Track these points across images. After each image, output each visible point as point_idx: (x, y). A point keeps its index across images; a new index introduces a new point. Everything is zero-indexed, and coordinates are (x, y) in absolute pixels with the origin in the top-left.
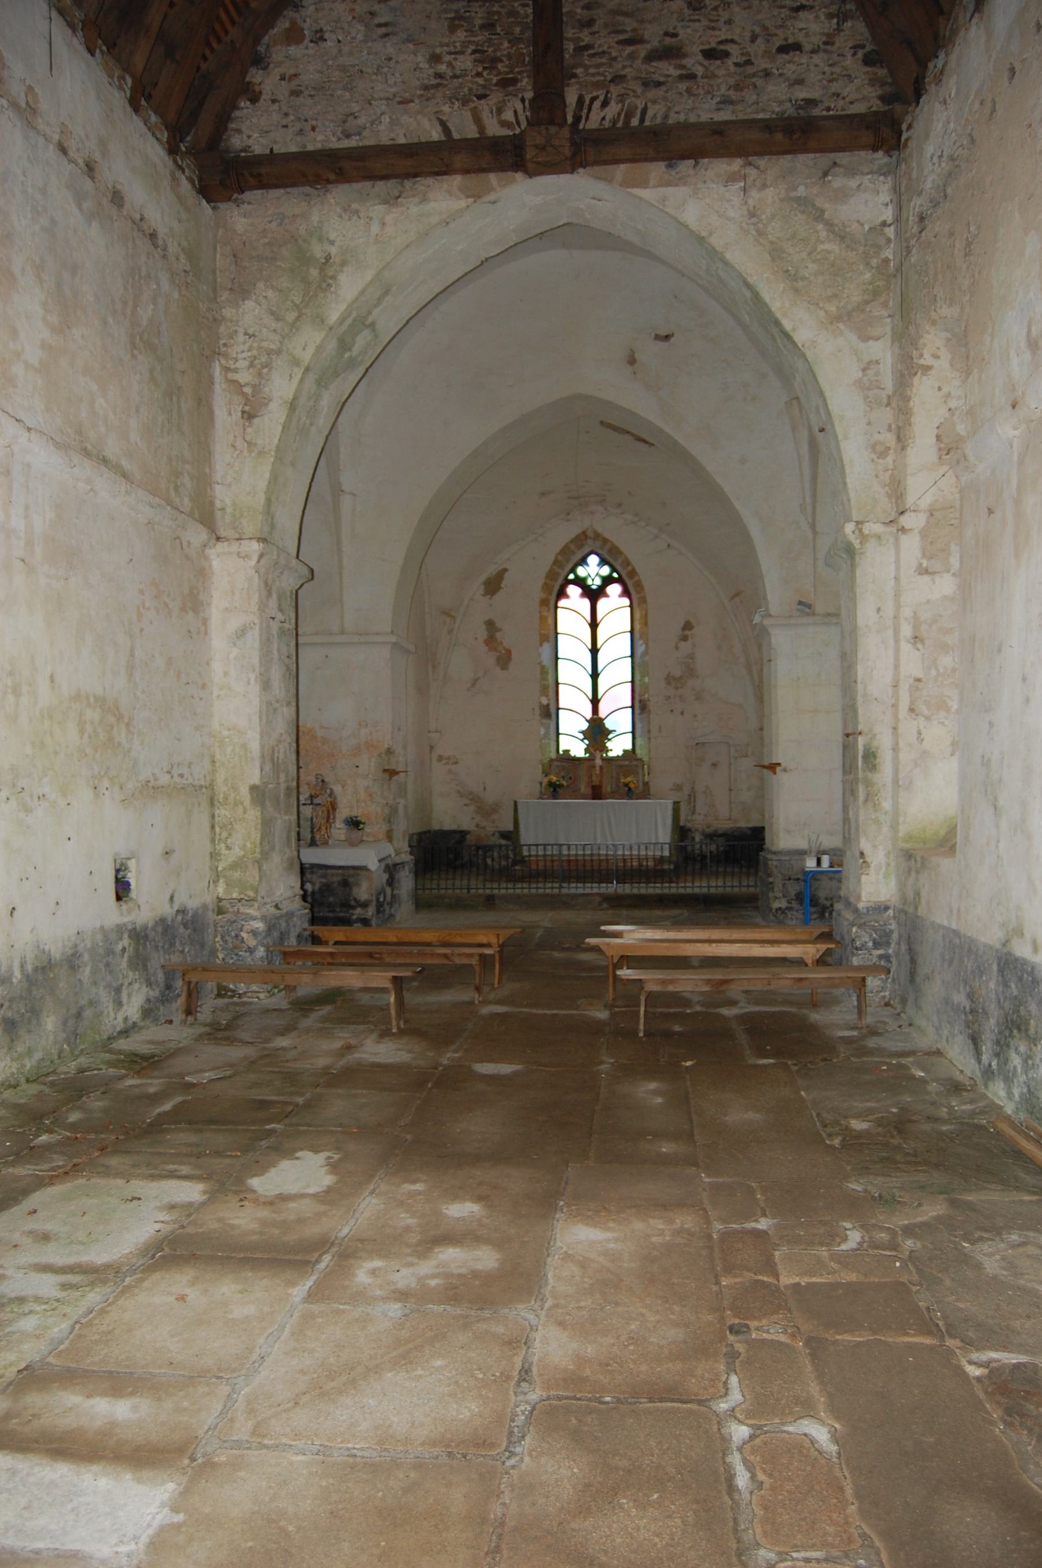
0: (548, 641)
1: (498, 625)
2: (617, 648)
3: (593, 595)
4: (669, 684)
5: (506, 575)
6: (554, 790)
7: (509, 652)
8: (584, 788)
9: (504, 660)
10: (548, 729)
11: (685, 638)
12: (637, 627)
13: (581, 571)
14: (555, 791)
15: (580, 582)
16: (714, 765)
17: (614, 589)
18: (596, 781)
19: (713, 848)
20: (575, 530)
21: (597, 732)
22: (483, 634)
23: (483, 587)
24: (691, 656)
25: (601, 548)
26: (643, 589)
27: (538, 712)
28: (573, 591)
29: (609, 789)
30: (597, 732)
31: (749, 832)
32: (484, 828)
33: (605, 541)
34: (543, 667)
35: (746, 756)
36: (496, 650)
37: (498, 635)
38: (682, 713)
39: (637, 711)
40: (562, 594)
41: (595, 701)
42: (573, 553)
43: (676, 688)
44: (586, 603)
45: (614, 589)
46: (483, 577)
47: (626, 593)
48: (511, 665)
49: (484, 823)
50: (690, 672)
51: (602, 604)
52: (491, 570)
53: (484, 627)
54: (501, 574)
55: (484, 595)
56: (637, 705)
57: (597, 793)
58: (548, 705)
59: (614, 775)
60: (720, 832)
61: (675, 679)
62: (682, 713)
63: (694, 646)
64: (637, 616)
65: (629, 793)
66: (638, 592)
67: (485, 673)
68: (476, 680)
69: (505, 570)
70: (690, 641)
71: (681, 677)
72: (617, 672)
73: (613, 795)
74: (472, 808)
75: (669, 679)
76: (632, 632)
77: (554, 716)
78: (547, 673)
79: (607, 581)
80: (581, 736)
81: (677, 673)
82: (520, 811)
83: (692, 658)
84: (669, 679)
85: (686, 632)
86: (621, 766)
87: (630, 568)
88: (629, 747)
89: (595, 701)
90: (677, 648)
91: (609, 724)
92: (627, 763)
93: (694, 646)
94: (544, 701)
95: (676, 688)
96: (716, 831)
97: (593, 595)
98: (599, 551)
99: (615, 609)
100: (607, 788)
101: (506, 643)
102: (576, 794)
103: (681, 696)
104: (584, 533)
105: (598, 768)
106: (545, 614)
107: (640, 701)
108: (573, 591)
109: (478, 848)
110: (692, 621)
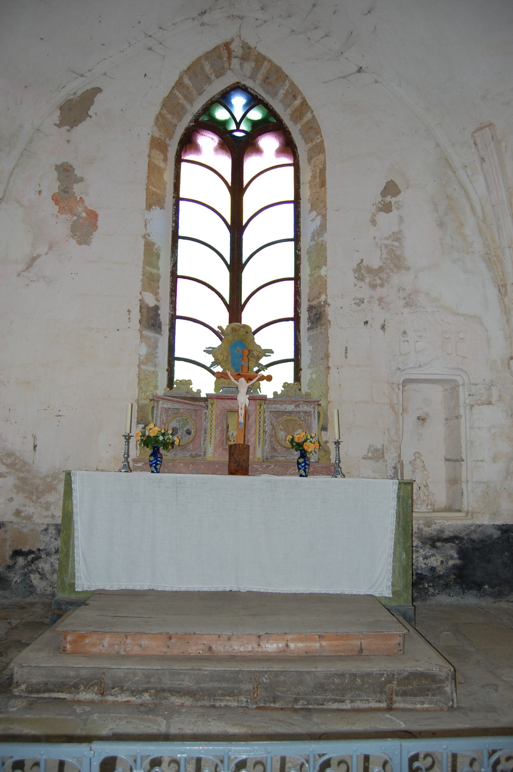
0: (162, 208)
1: (78, 172)
2: (271, 226)
3: (238, 147)
4: (361, 278)
5: (99, 98)
6: (156, 452)
7: (93, 216)
8: (214, 451)
9: (85, 227)
10: (154, 347)
11: (387, 208)
12: (306, 193)
13: (221, 114)
14: (155, 453)
15: (218, 128)
16: (422, 419)
17: (269, 143)
18: (235, 436)
19: (435, 561)
20: (209, 41)
21: (238, 351)
22: (51, 184)
23: (58, 113)
24: (397, 237)
25: (253, 77)
26: (318, 132)
27: (136, 316)
28: (207, 141)
29: (259, 454)
30: (238, 351)
31: (497, 534)
32: (29, 518)
33: (260, 59)
34: (149, 246)
35: (490, 403)
36: (71, 211)
37: (77, 188)
38: (383, 327)
39: (304, 324)
40: (188, 143)
41: (235, 306)
42: (209, 81)
43: (373, 286)
44: (224, 163)
45: (269, 143)
46: (61, 97)
47: (288, 147)
48: (96, 237)
49: (30, 510)
50: (396, 261)
51: (251, 165)
52: (76, 87)
53: (55, 174)
54: (89, 97)
55: (59, 126)
56: (304, 315)
57: (238, 463)
58: (156, 308)
59: (268, 428)
60: (447, 534)
61: (370, 270)
62: (383, 327)
63: (401, 220)
64: (306, 177)
65: (304, 465)
66: (307, 140)
67: (50, 248)
68: (34, 259)
69: (98, 90)
70: (395, 213)
71: (381, 269)
72: (271, 264)
73: (273, 466)
74: (10, 481)
75: (361, 271)
76: (297, 202)
77: (166, 328)
78: (158, 256)
79: (259, 129)
80: (208, 360)
81: (375, 263)
82: (76, 494)
83: (398, 240)
84: (361, 271)
85: (389, 199)
86: (279, 414)
87: (297, 102)
88: (291, 380)
89: (235, 306)
90: (374, 222)
91: (261, 340)
92: (291, 408)
93: (401, 220)
94: (150, 301)
95: (373, 286)
96: (442, 531)
97: (238, 147)
98: (249, 83)
99: (271, 177)
100: (257, 453)
101: (90, 202)
102: (200, 465)
103: (380, 300)
104: (227, 45)
105: (242, 412)
106: (159, 161)
107: (310, 308)
108: (207, 141)
109: (17, 553)
110: (398, 182)
